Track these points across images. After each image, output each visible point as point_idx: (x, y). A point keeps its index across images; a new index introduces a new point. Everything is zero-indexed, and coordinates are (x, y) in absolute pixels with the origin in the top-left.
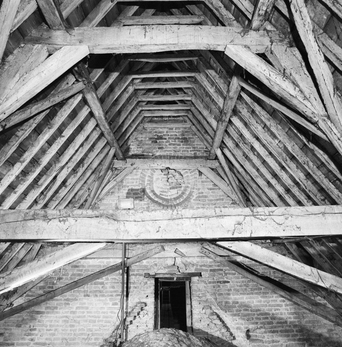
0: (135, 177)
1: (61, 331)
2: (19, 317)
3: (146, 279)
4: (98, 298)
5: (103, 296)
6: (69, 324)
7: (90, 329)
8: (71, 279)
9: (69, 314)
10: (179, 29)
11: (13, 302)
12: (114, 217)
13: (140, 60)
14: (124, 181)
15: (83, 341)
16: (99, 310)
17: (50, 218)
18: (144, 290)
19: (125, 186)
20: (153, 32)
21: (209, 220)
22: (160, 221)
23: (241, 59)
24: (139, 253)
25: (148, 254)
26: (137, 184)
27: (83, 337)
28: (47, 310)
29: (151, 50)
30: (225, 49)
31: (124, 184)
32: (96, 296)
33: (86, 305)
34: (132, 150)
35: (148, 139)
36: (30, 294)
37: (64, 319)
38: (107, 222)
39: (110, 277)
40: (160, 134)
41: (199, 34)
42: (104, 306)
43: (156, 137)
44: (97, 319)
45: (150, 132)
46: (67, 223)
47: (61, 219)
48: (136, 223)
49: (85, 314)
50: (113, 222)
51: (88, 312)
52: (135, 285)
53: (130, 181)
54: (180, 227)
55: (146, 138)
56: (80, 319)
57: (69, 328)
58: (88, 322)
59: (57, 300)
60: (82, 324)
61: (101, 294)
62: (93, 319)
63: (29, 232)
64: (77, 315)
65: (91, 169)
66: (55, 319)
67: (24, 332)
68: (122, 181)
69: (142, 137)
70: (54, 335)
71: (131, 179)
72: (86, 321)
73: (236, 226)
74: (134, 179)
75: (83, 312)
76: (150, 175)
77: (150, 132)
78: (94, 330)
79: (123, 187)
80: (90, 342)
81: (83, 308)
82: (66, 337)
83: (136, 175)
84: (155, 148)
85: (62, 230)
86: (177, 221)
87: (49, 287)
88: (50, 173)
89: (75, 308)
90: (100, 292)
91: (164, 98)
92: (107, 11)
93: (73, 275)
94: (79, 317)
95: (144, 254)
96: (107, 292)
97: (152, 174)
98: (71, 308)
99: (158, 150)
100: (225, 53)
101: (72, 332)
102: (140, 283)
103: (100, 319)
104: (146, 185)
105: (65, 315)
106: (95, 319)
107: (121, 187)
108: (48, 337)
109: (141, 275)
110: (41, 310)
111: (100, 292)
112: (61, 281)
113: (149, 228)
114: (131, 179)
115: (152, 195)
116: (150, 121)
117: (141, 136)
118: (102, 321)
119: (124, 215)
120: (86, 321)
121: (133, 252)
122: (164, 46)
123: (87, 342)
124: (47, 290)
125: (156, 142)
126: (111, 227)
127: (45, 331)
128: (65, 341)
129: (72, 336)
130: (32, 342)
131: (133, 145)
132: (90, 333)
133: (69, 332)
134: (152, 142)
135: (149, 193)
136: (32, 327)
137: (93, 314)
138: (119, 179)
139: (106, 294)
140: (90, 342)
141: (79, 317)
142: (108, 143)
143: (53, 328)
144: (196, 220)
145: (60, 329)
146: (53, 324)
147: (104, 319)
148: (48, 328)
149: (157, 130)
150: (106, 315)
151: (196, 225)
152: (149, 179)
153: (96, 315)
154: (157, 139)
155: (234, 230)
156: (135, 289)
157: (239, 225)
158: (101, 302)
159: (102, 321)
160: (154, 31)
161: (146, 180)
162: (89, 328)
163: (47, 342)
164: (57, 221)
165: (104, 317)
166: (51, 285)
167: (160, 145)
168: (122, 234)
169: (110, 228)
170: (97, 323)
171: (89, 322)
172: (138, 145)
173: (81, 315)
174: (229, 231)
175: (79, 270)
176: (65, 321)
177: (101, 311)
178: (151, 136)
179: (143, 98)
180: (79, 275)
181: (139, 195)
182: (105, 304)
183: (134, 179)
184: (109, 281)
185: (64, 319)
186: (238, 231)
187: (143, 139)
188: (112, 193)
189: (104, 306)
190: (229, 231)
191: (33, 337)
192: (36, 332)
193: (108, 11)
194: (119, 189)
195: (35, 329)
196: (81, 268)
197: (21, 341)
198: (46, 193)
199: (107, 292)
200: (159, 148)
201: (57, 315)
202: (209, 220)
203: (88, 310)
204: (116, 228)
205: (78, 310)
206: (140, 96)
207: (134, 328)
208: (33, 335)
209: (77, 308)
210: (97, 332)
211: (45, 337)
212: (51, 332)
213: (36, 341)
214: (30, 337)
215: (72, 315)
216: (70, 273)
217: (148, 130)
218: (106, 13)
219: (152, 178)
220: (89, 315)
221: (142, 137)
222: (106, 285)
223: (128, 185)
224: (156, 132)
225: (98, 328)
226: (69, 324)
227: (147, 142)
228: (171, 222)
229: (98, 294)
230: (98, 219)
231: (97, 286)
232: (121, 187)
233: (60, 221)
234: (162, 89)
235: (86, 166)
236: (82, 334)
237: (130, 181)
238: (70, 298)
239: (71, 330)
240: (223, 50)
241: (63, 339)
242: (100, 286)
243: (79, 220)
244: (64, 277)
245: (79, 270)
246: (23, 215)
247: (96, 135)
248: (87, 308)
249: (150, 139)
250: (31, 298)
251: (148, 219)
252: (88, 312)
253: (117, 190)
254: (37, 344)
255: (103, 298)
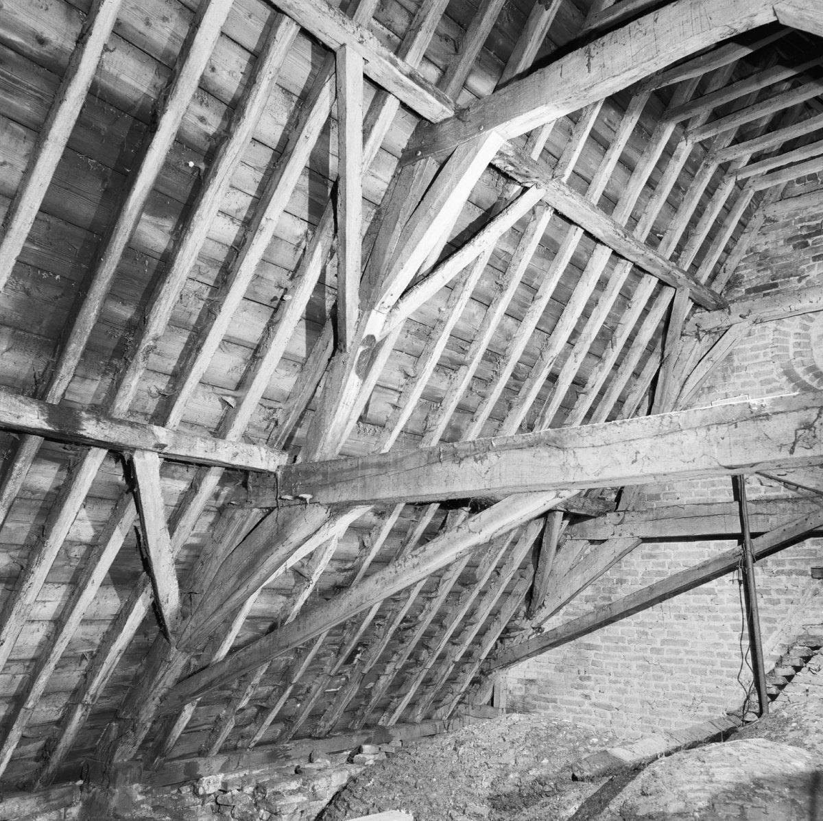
0: (762, 343)
1: (636, 687)
2: (558, 652)
3: (818, 581)
4: (705, 623)
5: (716, 618)
6: (651, 673)
7: (696, 687)
8: (644, 581)
9: (648, 654)
10: (656, 21)
11: (541, 623)
12: (559, 443)
13: (671, 82)
14: (735, 357)
15: (685, 710)
16: (712, 649)
17: (462, 455)
18: (813, 609)
19: (738, 368)
20: (605, 51)
21: (736, 427)
22: (638, 442)
23: (817, 25)
24: (786, 520)
25: (809, 521)
26: (768, 359)
27: (683, 701)
28: (606, 644)
29: (612, 88)
30: (775, 15)
31: (736, 364)
32: (701, 618)
33: (682, 638)
34: (745, 279)
35: (781, 242)
36: (571, 610)
37: (641, 662)
38: (546, 454)
39: (730, 576)
40: (813, 223)
41: (702, 11)
42: (721, 641)
43: (804, 232)
44: (709, 668)
45: (787, 225)
46: (486, 462)
47: (477, 456)
48: (595, 450)
49: (681, 656)
50: (556, 452)
51: (687, 652)
52: (791, 597)
53: (750, 353)
54: (676, 449)
55: (776, 242)
56: (672, 665)
57: (653, 683)
58: (690, 673)
59: (623, 624)
60: (677, 675)
61: (710, 614)
62: (699, 666)
63: (435, 482)
64: (666, 656)
65: (639, 345)
66: (623, 661)
67: (570, 682)
68: (729, 358)
69: (766, 243)
70: (624, 692)
71: (752, 350)
72: (686, 670)
73: (800, 432)
74: (758, 348)
75: (678, 652)
76: (802, 331)
77: (787, 225)
78: (704, 690)
79: (733, 371)
80: (699, 713)
81: (675, 642)
82: (648, 698)
83: (762, 337)
84: (803, 262)
85: (480, 474)
86: (670, 438)
87: (604, 598)
88: (537, 372)
89: (659, 640)
90: (709, 609)
91: (780, 138)
92: (543, 31)
93: (647, 573)
94: (669, 661)
95: (797, 522)
96: (723, 610)
97: (806, 328)
98: (652, 641)
99: (812, 263)
100: (781, 22)
101: (660, 690)
102: (803, 592)
103: (715, 668)
104: (792, 356)
105: (641, 654)
106: (704, 667)
107: (729, 371)
108: (615, 694)
109: (803, 573)
110: (595, 643)
111: (709, 609)
112: (625, 585)
113: (618, 456)
114: (752, 350)
115: (811, 380)
116: (783, 198)
117: (763, 240)
118: (720, 672)
119: (574, 436)
120: (686, 670)
121: (771, 519)
122: (632, 71)
123: (692, 712)
124: (601, 603)
125: (806, 245)
126: (555, 462)
127: (608, 684)
128: (647, 707)
129: (661, 698)
130: (587, 702)
131: (745, 268)
132: (698, 695)
133: (653, 689)
134: (795, 247)
135: (801, 375)
136: (582, 674)
137: (699, 657)
138: (719, 352)
139: (722, 616)
140: (699, 713)
141: (669, 661)
142: (662, 284)
143: (622, 680)
144: (709, 430)
145: (635, 681)
146: (619, 670)
147: (725, 669)
148: (613, 677)
149: (804, 214)
150: (726, 659)
151: (709, 441)
152: (799, 341)
153: (706, 658)
154: (809, 236)
155: (794, 443)
156: (790, 606)
157: (807, 431)
158: (713, 632)
159: (720, 672)
160: (607, 51)
161: (791, 346)
162: (693, 684)
163: (615, 704)
164: (471, 460)
165: (723, 664)
166: (607, 595)
167: (817, 249)
168: (572, 472)
169: (553, 464)
170: (709, 676)
171: (693, 672)
172: (760, 265)
173: (673, 656)
174: (781, 446)
175: (658, 565)
176: (641, 666)
177: (716, 651)
178: (789, 232)
179: (727, 154)
180: (659, 573)
181: (775, 384)
182: (723, 636)
183: (758, 348)
184: (726, 587)
185: (641, 662)
186: (805, 445)
187: (770, 246)
188: (709, 388)
189: (721, 641)
190: (781, 446)
191: (587, 692)
192: (591, 683)
193: (547, 29)
194: (724, 378)
195: (589, 678)
196: (661, 560)
197: (567, 697)
198: (544, 412)
199: (723, 610)
200: (815, 259)
201: (626, 653)
202: (736, 427)
203: (687, 648)
204: (561, 463)
205: (666, 647)
206: (719, 153)
207: (799, 694)
208: (586, 687)
209: (664, 642)
210: (712, 695)
211: (608, 694)
212: (618, 686)
213: (594, 700)
214: (581, 691)
215: (654, 656)
216: (641, 570)
217: (781, 221)
218: (544, 36)
219: (808, 337)
220: (690, 657)
221: (766, 243)
222: (720, 596)
223: (746, 364)
224: (801, 220)
225: (714, 686)
226: (651, 673)
227: (781, 252)
228: (659, 440)
229: (706, 615)
230: (533, 451)
231: (699, 596)
232: (729, 371)
233: (476, 460)
234: (793, 107)
235: (620, 343)
236: (681, 696)
237: (750, 353)
238: (646, 620)
239: (656, 686)
240: (774, 19)
241: (642, 702)
242: (708, 598)
243: (504, 456)
244: (629, 578)
245: (658, 565)
246: (426, 456)
247: (622, 273)
248: (685, 643)
249: (790, 240)
250: (572, 618)
251: (616, 439)
252: (687, 652)
253: (720, 380)
254: (595, 705)
255: (717, 624)
